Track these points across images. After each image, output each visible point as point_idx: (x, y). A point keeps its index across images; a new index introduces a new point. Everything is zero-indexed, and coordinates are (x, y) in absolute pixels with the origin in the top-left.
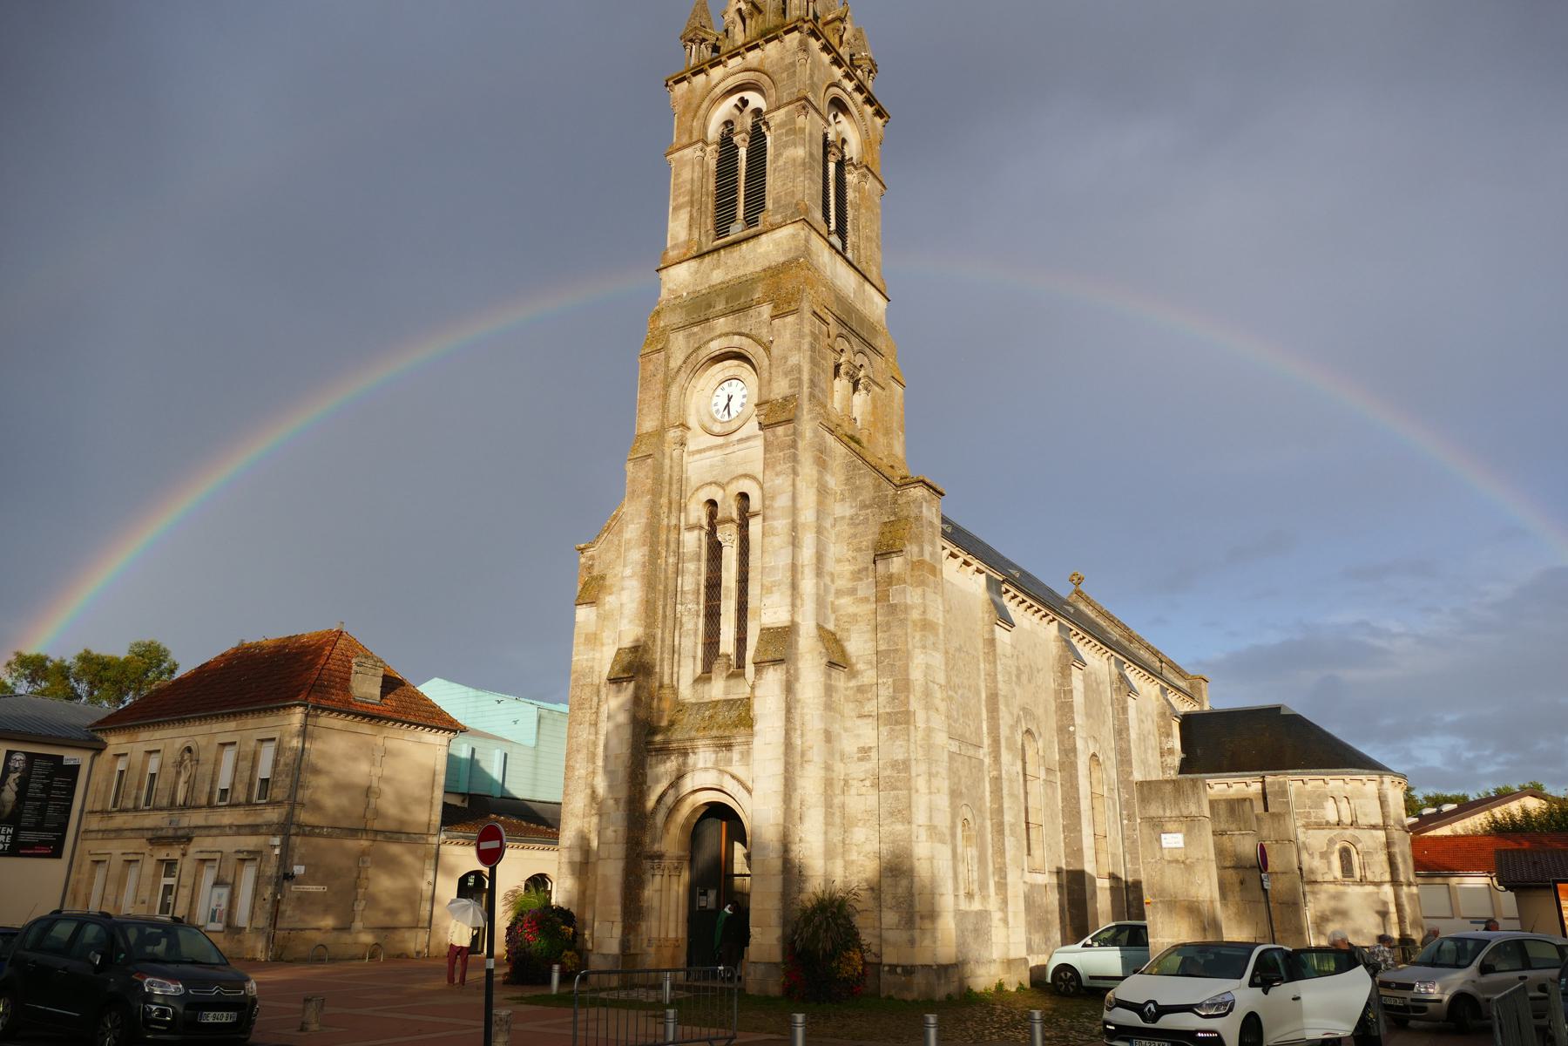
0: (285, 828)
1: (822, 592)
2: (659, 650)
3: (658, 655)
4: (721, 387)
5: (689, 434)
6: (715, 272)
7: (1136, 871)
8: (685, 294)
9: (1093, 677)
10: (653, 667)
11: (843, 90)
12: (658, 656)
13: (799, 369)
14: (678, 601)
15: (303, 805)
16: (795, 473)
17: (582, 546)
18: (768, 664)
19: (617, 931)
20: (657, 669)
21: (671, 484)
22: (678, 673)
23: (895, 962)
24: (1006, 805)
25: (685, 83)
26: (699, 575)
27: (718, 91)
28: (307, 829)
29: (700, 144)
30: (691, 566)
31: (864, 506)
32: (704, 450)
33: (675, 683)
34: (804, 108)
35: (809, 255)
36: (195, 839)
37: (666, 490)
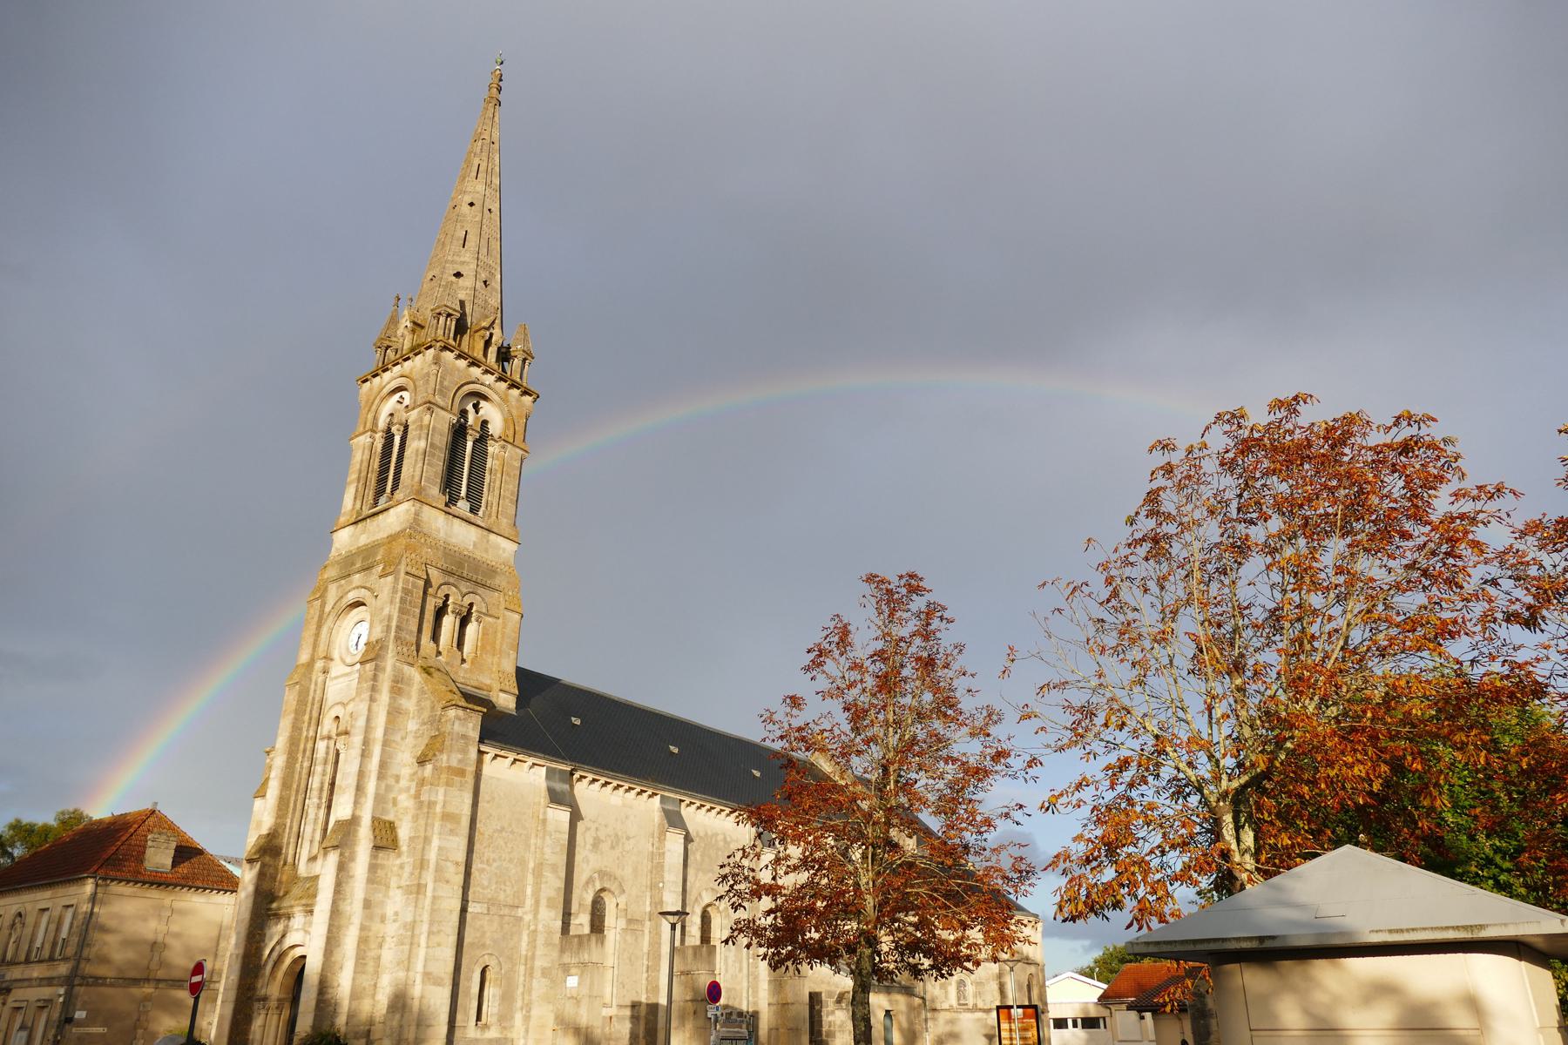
0: (69, 981)
3: (287, 839)
5: (332, 664)
7: (756, 1003)
9: (720, 837)
10: (281, 849)
13: (390, 618)
15: (88, 960)
16: (372, 699)
17: (268, 749)
20: (284, 851)
21: (313, 704)
24: (538, 953)
27: (386, 391)
28: (91, 980)
31: (424, 724)
34: (429, 409)
35: (419, 525)
36: (13, 991)
37: (308, 709)
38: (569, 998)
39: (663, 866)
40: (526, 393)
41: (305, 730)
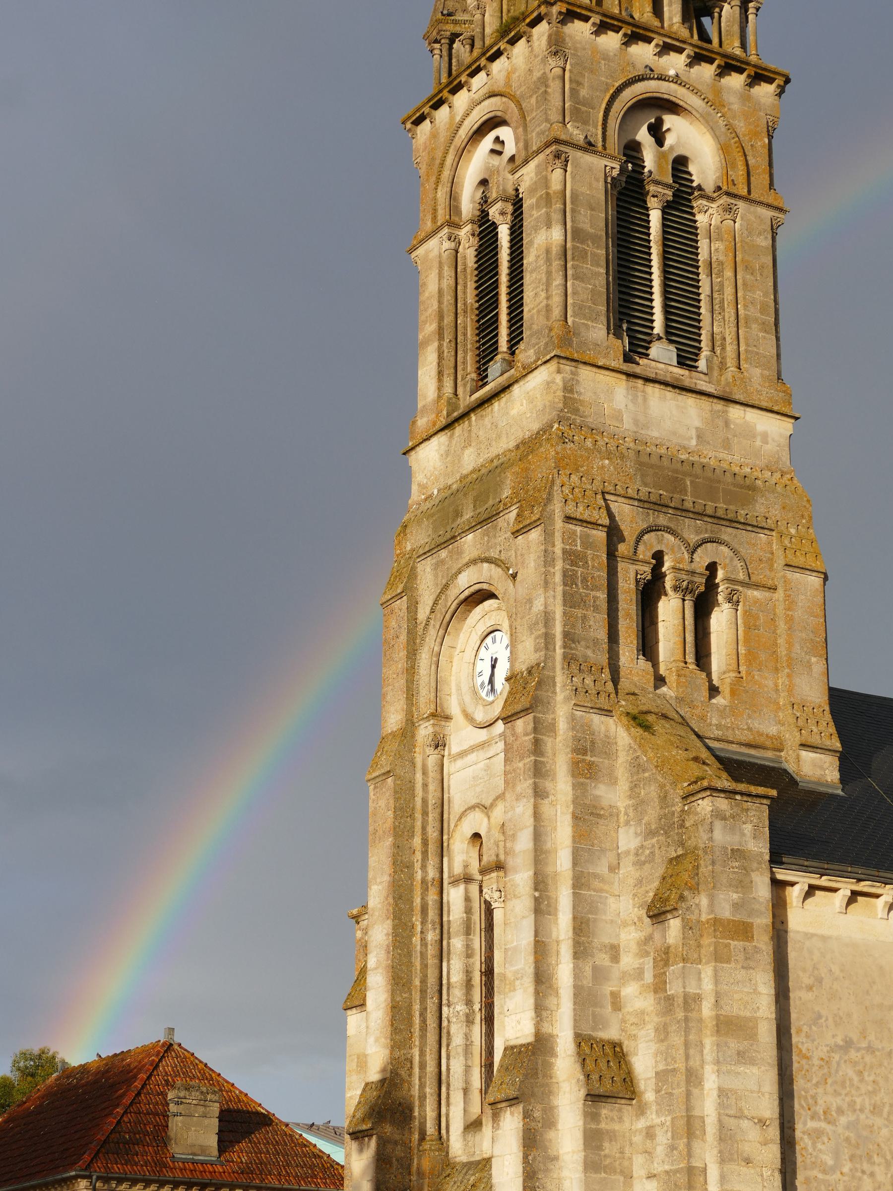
1: (587, 982)
2: (417, 1082)
4: (484, 644)
5: (451, 727)
6: (468, 452)
8: (436, 492)
10: (411, 1110)
11: (659, 79)
12: (415, 1091)
13: (547, 619)
14: (444, 1001)
18: (504, 1104)
20: (416, 1114)
21: (425, 813)
25: (482, 74)
27: (464, 133)
29: (446, 230)
30: (457, 943)
34: (557, 156)
35: (576, 411)
37: (419, 824)
40: (759, 77)
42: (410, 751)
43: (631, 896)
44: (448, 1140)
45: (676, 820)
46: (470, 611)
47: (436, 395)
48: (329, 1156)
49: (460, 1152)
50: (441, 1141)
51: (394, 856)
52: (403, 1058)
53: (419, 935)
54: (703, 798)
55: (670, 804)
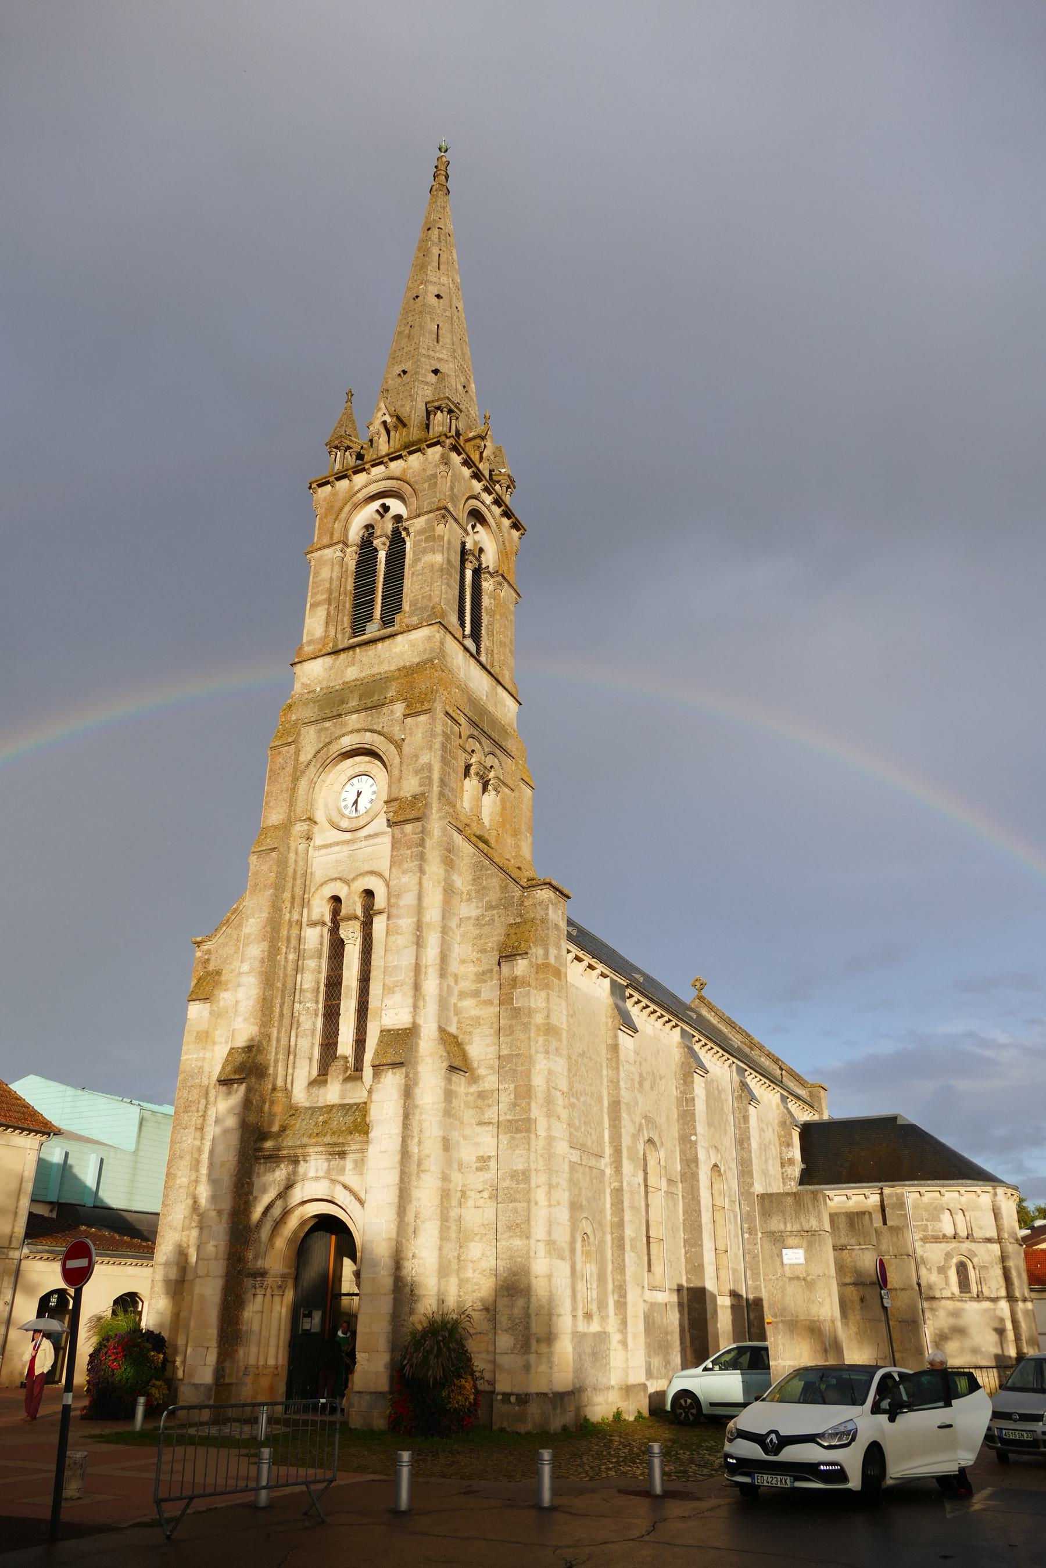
1: (445, 994)
2: (274, 1050)
3: (273, 1055)
4: (351, 782)
7: (757, 1288)
8: (318, 689)
10: (267, 1068)
11: (482, 502)
12: (272, 1057)
13: (429, 767)
17: (199, 939)
18: (387, 1067)
19: (212, 1358)
20: (271, 1071)
21: (294, 879)
22: (293, 1075)
23: (508, 1389)
24: (627, 1219)
26: (320, 972)
27: (361, 496)
32: (330, 845)
33: (289, 1086)
34: (444, 517)
35: (444, 657)
37: (290, 884)
38: (791, 1279)
39: (693, 1115)
40: (516, 526)
41: (286, 912)
42: (287, 838)
43: (470, 945)
44: (292, 1091)
45: (515, 901)
46: (342, 761)
47: (323, 634)
48: (33, 1107)
49: (302, 1100)
50: (288, 1093)
51: (273, 902)
52: (265, 1033)
53: (284, 954)
54: (541, 890)
55: (510, 891)
